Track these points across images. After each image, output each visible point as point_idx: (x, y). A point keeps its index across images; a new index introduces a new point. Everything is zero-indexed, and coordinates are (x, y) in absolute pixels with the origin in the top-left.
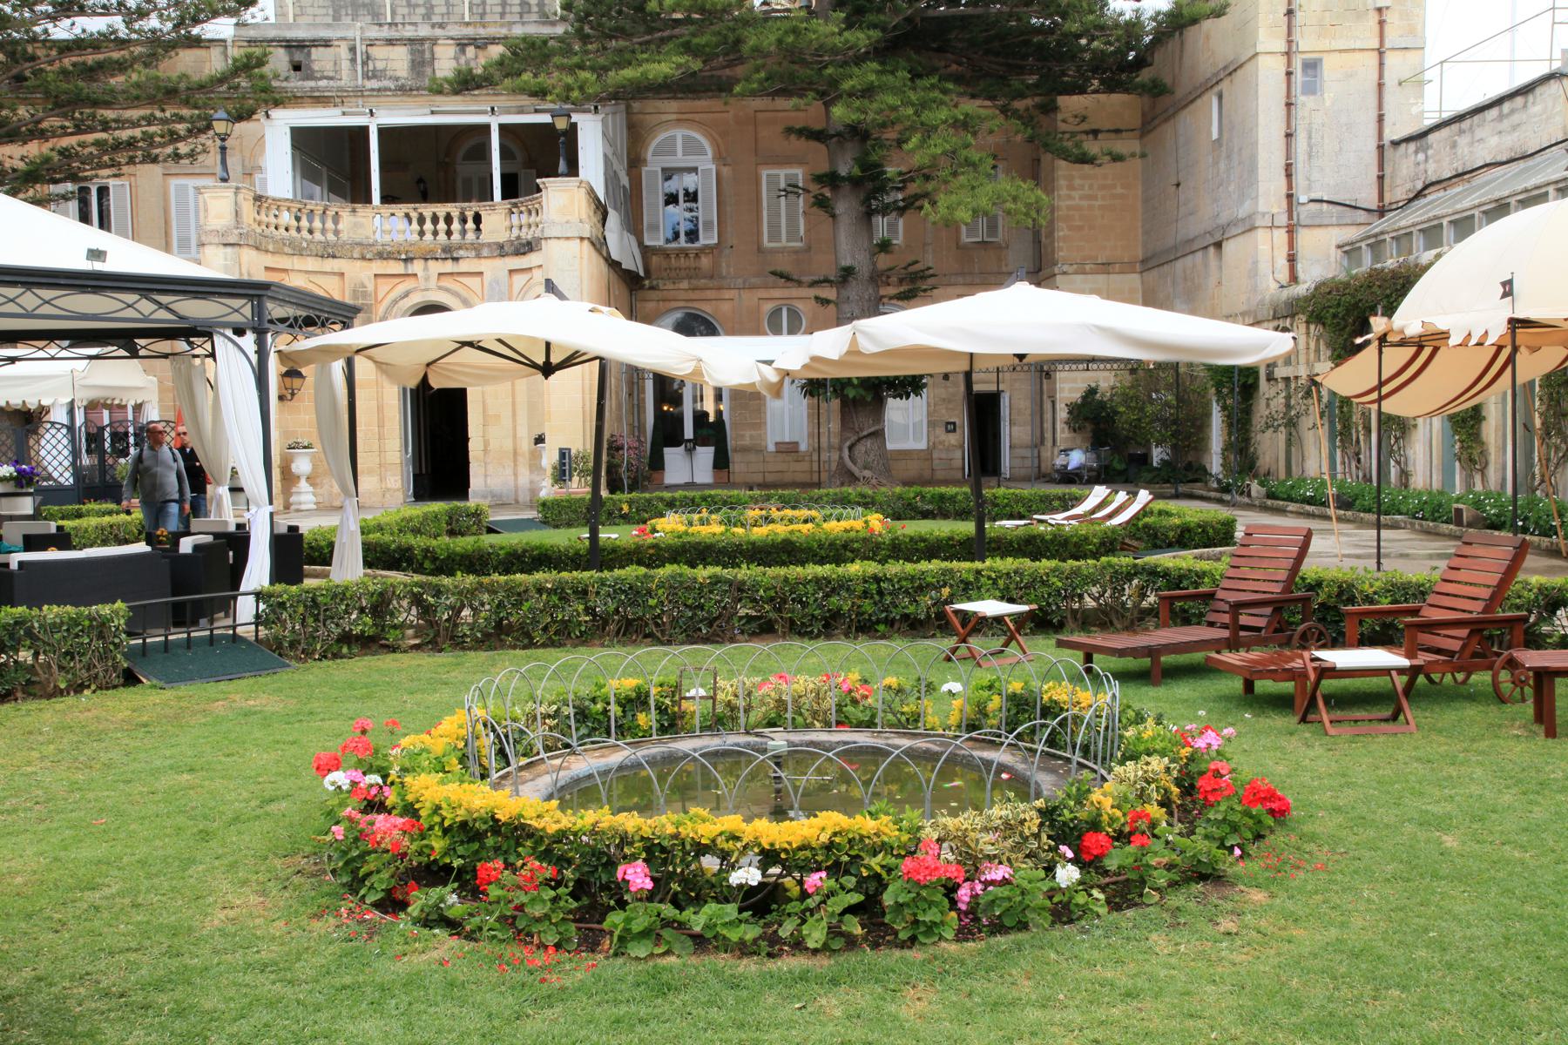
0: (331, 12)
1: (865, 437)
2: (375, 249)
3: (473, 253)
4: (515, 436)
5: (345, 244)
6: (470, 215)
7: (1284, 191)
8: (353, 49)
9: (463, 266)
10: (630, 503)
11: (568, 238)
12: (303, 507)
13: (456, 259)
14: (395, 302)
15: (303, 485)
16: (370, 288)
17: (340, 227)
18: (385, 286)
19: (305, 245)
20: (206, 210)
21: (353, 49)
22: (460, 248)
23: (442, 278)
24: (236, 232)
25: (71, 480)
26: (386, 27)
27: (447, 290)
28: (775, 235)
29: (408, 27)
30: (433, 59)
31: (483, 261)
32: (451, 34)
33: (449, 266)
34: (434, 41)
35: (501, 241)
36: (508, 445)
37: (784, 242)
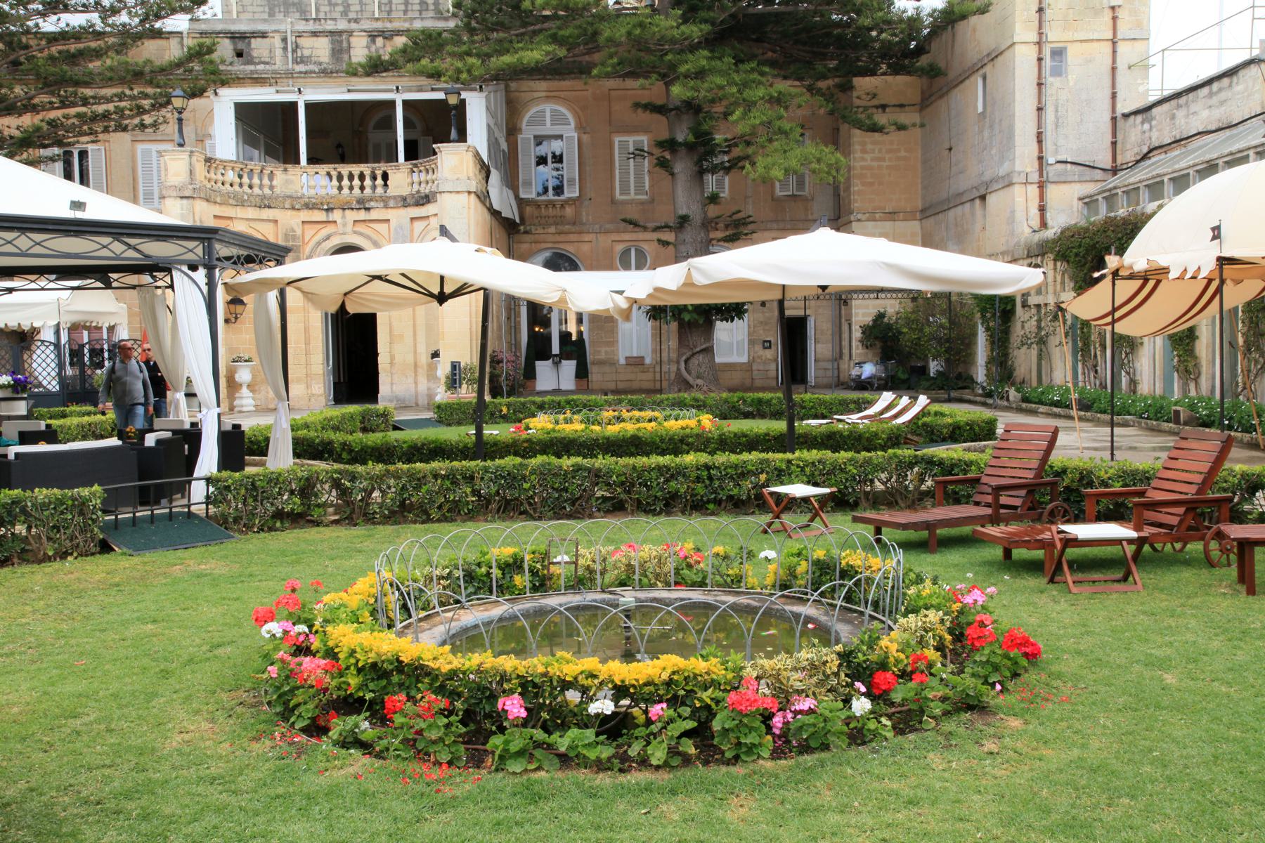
0: (267, 9)
1: (698, 352)
2: (302, 201)
3: (382, 204)
4: (415, 352)
5: (278, 197)
6: (379, 173)
7: (1036, 154)
8: (285, 40)
9: (374, 215)
10: (508, 405)
11: (458, 192)
12: (245, 409)
13: (368, 209)
14: (319, 244)
15: (245, 391)
16: (299, 232)
17: (275, 183)
18: (310, 231)
19: (246, 197)
20: (166, 170)
21: (285, 40)
22: (371, 200)
23: (357, 224)
24: (191, 187)
25: (57, 387)
26: (312, 22)
27: (361, 234)
28: (625, 190)
29: (329, 22)
30: (349, 47)
31: (390, 210)
32: (364, 27)
33: (362, 215)
34: (350, 33)
35: (404, 194)
36: (410, 359)
37: (632, 196)
